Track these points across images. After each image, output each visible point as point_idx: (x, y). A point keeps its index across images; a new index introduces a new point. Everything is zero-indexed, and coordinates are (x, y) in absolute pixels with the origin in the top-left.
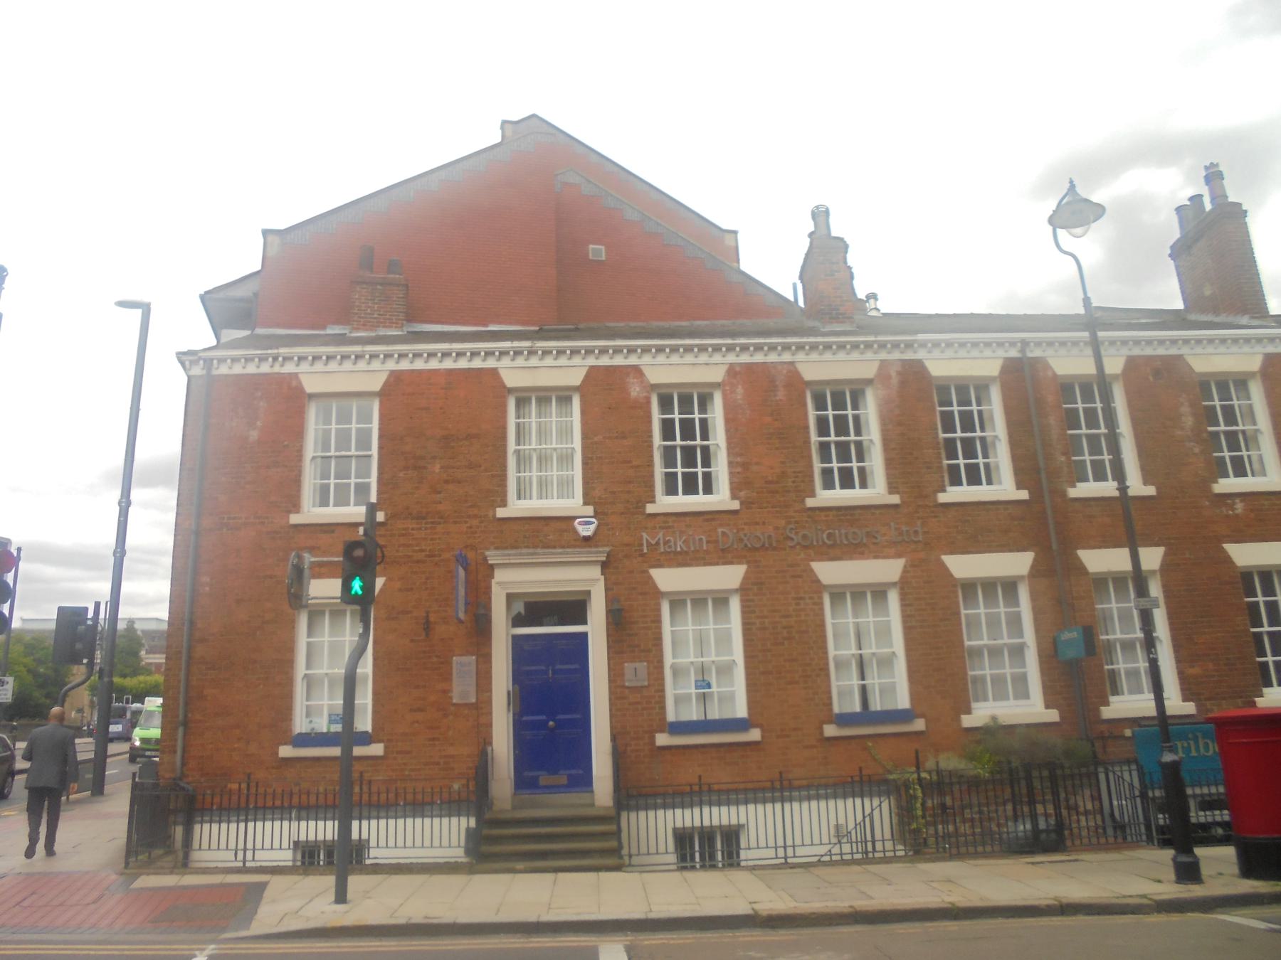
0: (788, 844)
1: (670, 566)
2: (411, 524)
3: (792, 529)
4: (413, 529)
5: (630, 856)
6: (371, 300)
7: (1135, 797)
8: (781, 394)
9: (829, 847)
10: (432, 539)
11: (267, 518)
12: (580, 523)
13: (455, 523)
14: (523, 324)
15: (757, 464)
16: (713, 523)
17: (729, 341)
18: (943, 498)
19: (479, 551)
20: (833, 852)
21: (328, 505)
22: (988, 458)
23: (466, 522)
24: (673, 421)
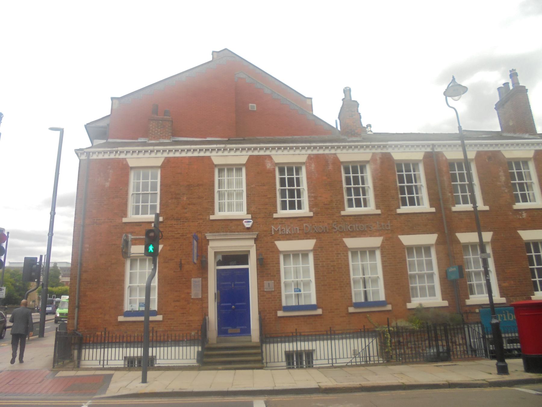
0: (333, 358)
1: (283, 240)
2: (174, 222)
3: (335, 224)
4: (175, 224)
5: (267, 363)
6: (157, 127)
7: (480, 338)
8: (330, 167)
9: (351, 359)
10: (183, 229)
11: (113, 220)
12: (245, 222)
13: (193, 222)
14: (221, 137)
15: (320, 197)
16: (302, 222)
17: (309, 145)
18: (399, 211)
19: (203, 234)
20: (352, 361)
21: (139, 214)
22: (418, 194)
23: (197, 221)
24: (285, 178)
